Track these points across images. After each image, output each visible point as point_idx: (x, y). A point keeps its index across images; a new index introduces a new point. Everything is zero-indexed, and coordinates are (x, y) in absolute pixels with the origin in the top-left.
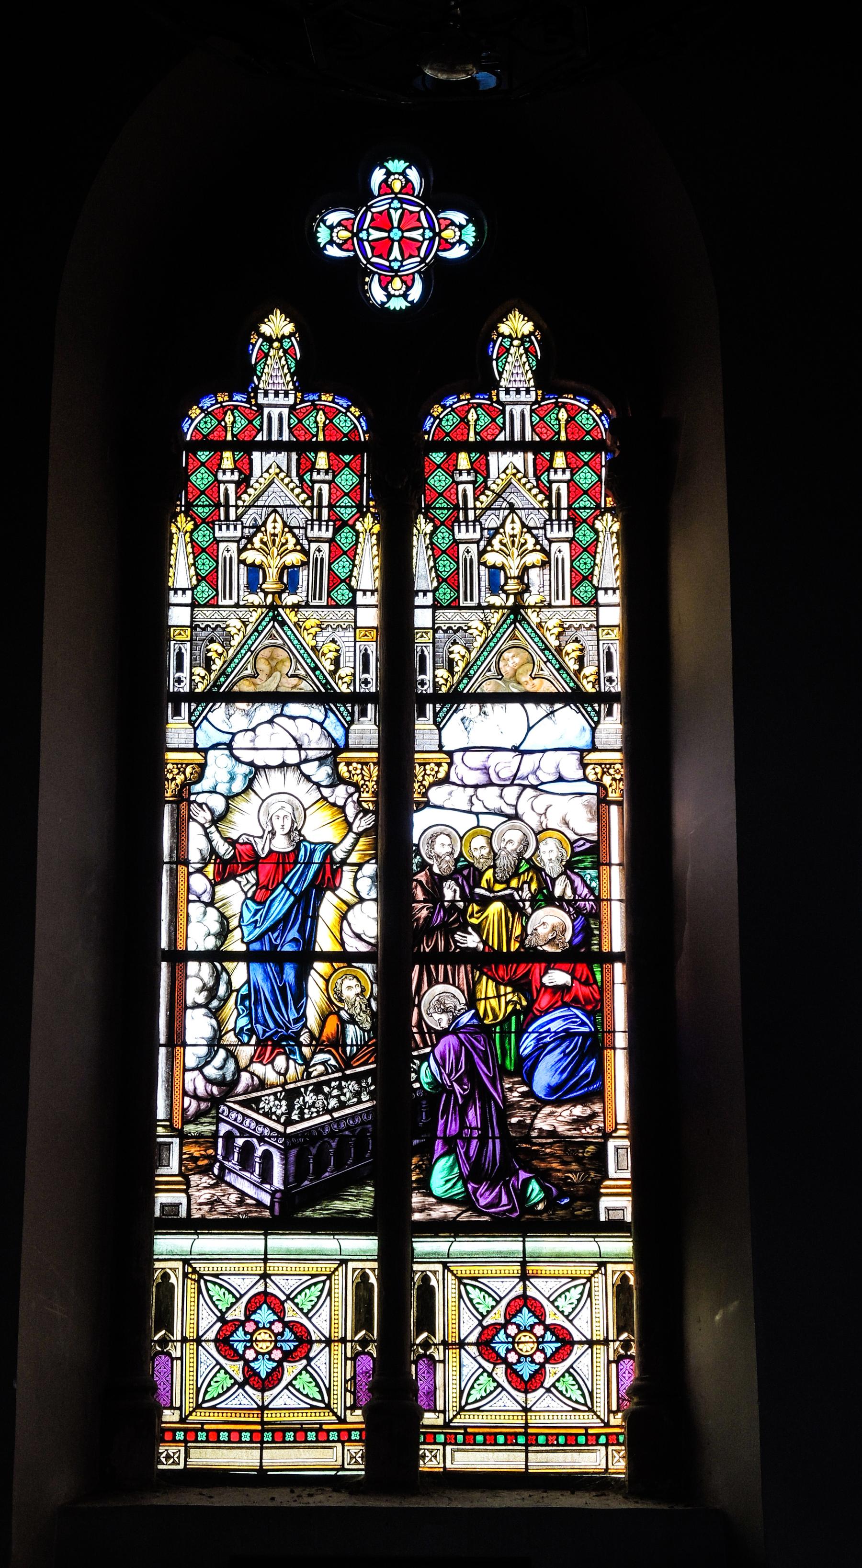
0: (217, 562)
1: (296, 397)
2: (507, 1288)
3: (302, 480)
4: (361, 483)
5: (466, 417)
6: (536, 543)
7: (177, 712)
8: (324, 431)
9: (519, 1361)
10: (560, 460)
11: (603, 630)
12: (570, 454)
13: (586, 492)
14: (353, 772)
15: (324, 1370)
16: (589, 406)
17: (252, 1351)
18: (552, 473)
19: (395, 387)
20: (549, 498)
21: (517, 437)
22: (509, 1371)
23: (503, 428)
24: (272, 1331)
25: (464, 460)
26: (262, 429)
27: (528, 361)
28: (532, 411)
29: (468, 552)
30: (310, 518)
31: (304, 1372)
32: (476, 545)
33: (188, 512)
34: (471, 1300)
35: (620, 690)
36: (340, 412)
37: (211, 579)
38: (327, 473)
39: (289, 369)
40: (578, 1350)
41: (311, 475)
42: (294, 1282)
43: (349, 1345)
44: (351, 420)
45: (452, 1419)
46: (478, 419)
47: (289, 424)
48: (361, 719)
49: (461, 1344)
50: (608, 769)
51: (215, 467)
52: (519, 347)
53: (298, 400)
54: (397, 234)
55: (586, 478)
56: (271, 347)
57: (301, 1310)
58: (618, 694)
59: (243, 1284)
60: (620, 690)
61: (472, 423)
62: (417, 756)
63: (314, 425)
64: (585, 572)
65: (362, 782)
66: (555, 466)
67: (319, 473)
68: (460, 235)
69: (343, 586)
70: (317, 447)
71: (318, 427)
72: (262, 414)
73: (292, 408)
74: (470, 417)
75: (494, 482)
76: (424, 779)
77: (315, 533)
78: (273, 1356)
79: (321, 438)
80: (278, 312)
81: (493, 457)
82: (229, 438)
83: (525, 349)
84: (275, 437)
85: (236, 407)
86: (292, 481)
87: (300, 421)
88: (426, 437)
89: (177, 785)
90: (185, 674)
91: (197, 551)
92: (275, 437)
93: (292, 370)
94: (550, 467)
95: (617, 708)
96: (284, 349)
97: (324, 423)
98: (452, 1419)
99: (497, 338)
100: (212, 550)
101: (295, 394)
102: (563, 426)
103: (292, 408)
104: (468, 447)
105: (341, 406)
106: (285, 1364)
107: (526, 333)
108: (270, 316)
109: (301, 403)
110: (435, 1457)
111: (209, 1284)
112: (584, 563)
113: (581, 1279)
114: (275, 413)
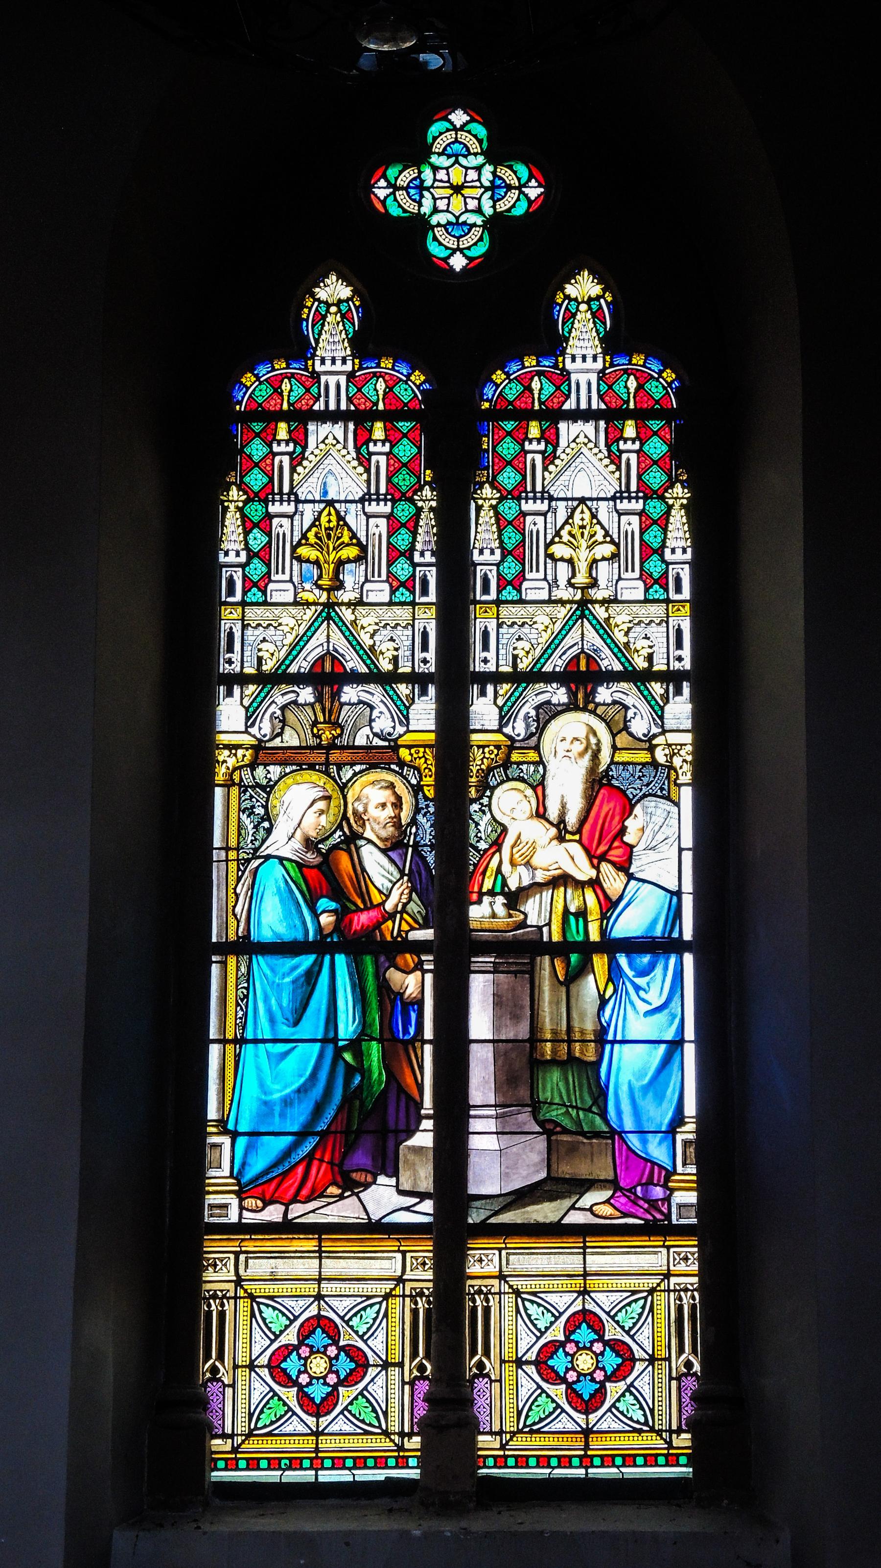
0: (523, 535)
2: (565, 1302)
4: (419, 452)
5: (280, 387)
6: (594, 517)
7: (230, 694)
10: (630, 430)
11: (673, 606)
12: (389, 425)
13: (509, 463)
14: (415, 756)
15: (380, 1394)
17: (306, 1375)
18: (371, 445)
19: (458, 348)
20: (368, 471)
21: (332, 406)
22: (569, 1391)
23: (568, 397)
24: (575, 1353)
25: (534, 430)
26: (320, 396)
27: (345, 328)
29: (535, 524)
30: (618, 489)
32: (543, 518)
34: (529, 1316)
35: (433, 671)
36: (401, 380)
38: (634, 442)
39: (347, 335)
41: (368, 448)
42: (303, 1302)
44: (412, 390)
45: (241, 1444)
46: (291, 390)
47: (599, 391)
49: (519, 1363)
50: (679, 750)
52: (336, 314)
53: (356, 367)
54: (457, 190)
55: (657, 448)
57: (622, 1328)
58: (430, 675)
59: (561, 1301)
60: (433, 671)
61: (285, 394)
62: (474, 737)
63: (375, 393)
64: (656, 546)
65: (425, 765)
66: (530, 436)
69: (655, 557)
72: (319, 382)
73: (351, 376)
74: (283, 387)
76: (483, 763)
78: (328, 1380)
79: (381, 406)
80: (586, 273)
81: (562, 426)
84: (583, 406)
85: (293, 375)
88: (238, 407)
93: (601, 336)
95: (432, 690)
96: (341, 314)
97: (385, 391)
98: (241, 1444)
99: (563, 302)
100: (265, 523)
102: (632, 396)
103: (351, 376)
104: (539, 416)
105: (402, 374)
106: (340, 1389)
107: (593, 295)
108: (577, 277)
111: (262, 1307)
112: (653, 537)
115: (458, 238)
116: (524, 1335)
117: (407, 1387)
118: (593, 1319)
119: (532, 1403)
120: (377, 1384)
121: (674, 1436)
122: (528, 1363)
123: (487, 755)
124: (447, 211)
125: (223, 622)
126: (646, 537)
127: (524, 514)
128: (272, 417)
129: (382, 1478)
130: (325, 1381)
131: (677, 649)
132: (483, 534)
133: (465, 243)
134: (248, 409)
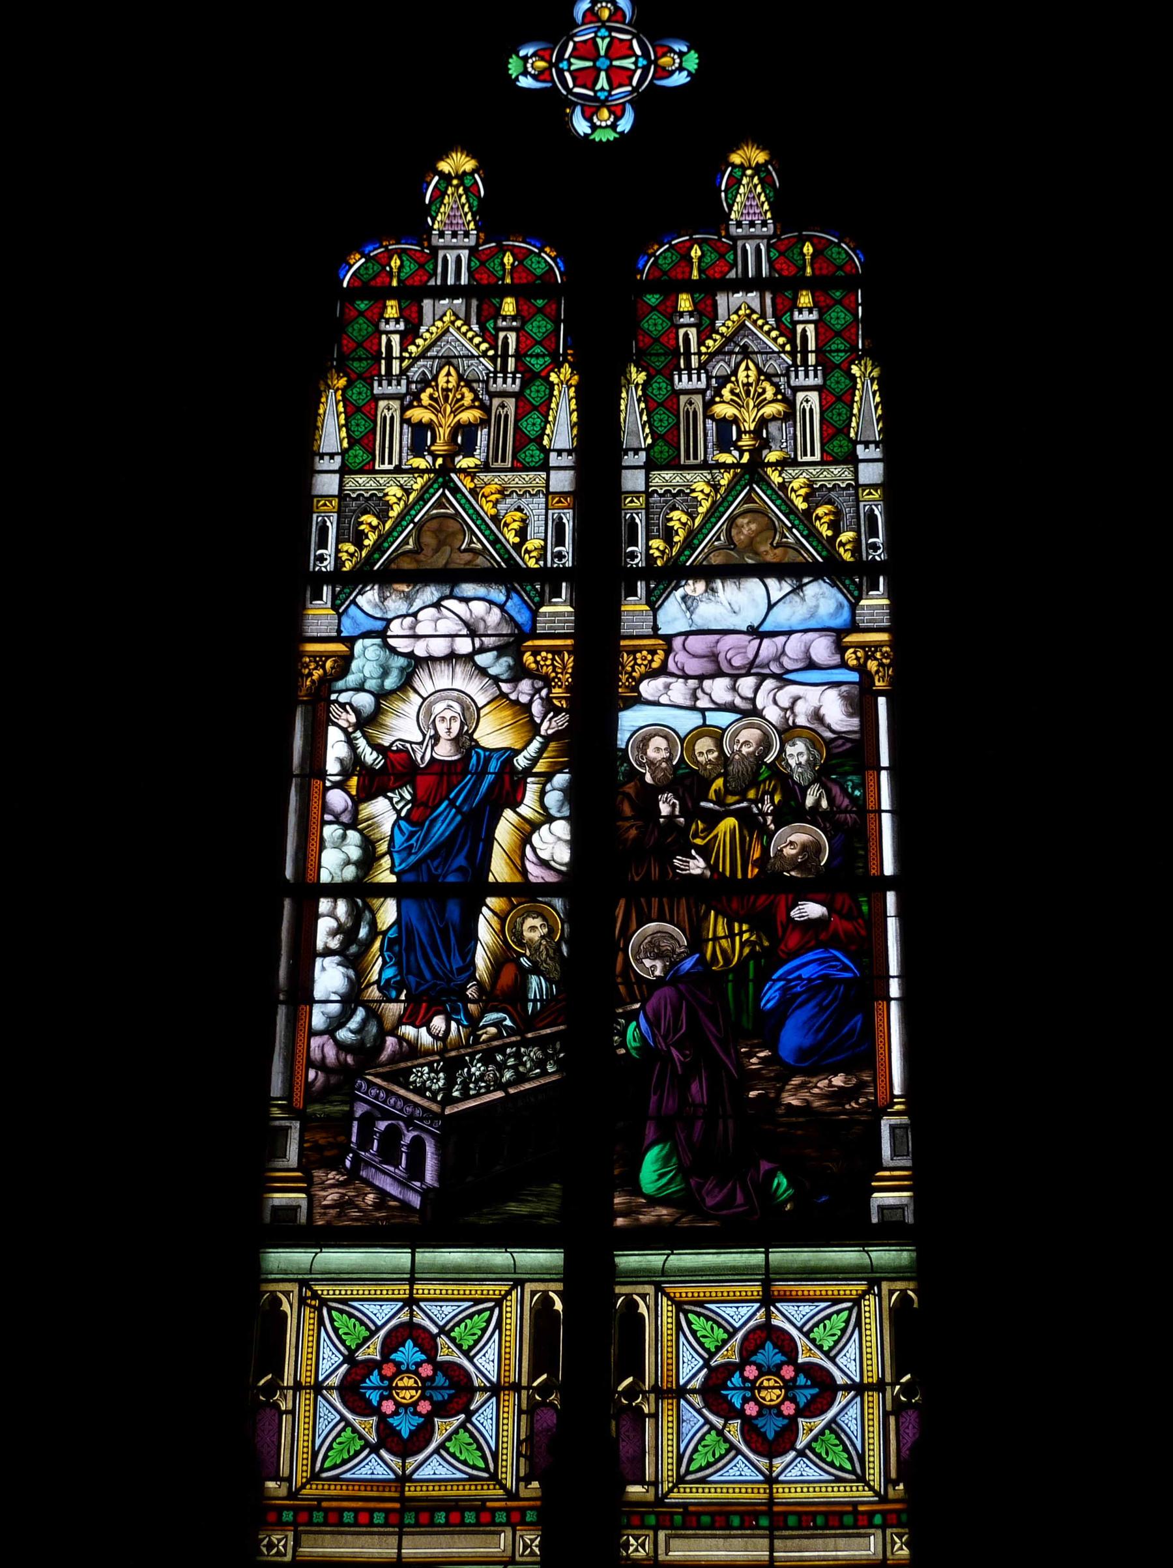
3: (483, 328)
19: (601, 261)
36: (533, 252)
38: (811, 312)
40: (841, 1399)
43: (524, 1393)
56: (744, 174)
67: (800, 312)
68: (682, 67)
69: (533, 446)
70: (506, 291)
73: (473, 251)
74: (693, 254)
76: (634, 670)
97: (512, 265)
101: (477, 235)
104: (690, 287)
114: (451, 256)
116: (327, 1353)
117: (524, 1417)
118: (423, 1335)
119: (699, 1442)
120: (849, 1413)
121: (522, 1484)
122: (484, 1389)
123: (639, 661)
125: (315, 516)
126: (523, 424)
127: (376, 399)
128: (381, 294)
130: (415, 1409)
131: (557, 546)
132: (632, 412)
134: (651, 277)
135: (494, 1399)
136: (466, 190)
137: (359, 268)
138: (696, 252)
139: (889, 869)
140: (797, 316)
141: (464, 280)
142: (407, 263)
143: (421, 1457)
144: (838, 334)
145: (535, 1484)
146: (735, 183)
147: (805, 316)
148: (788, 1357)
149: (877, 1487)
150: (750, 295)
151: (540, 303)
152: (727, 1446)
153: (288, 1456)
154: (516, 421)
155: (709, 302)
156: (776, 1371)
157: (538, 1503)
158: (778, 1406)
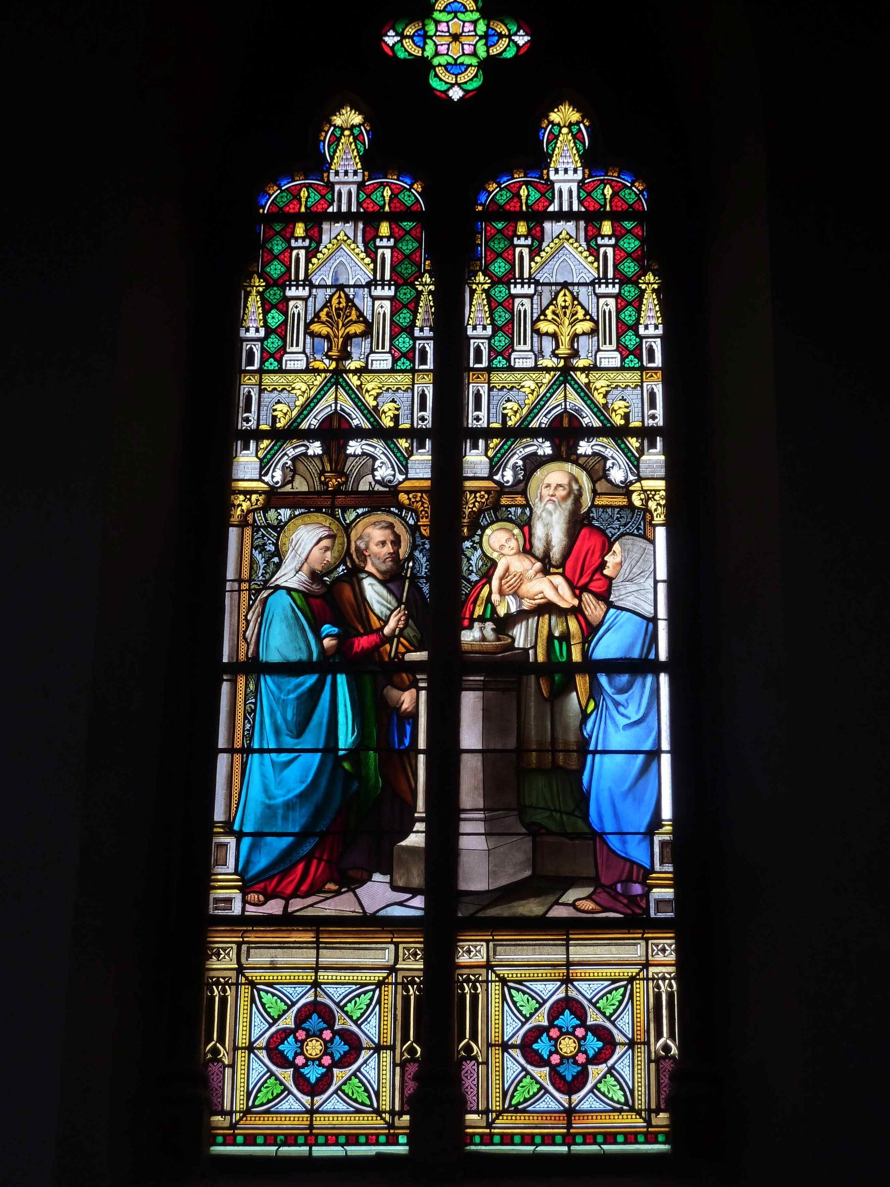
1: (364, 176)
3: (588, 245)
7: (475, 446)
8: (389, 204)
9: (561, 1063)
16: (633, 184)
19: (455, 191)
21: (565, 208)
24: (559, 1037)
28: (579, 188)
31: (608, 1076)
33: (263, 275)
36: (405, 188)
37: (281, 331)
39: (358, 152)
40: (517, 1040)
47: (579, 197)
48: (651, 451)
49: (505, 1047)
50: (654, 495)
51: (287, 236)
52: (349, 136)
53: (366, 178)
56: (342, 134)
59: (545, 989)
61: (303, 200)
67: (381, 240)
69: (630, 333)
70: (605, 216)
71: (605, 199)
73: (361, 186)
74: (521, 192)
75: (326, 247)
77: (602, 290)
81: (547, 225)
82: (303, 209)
83: (572, 135)
84: (565, 208)
86: (580, 245)
87: (368, 196)
88: (261, 211)
89: (242, 511)
90: (483, 414)
91: (492, 304)
92: (344, 209)
94: (377, 236)
97: (390, 197)
99: (547, 126)
100: (283, 305)
101: (363, 173)
109: (368, 180)
110: (228, 954)
111: (262, 993)
113: (626, 980)
114: (344, 190)
115: (456, 76)
121: (653, 1115)
122: (514, 1046)
124: (447, 54)
127: (513, 297)
128: (513, 217)
129: (374, 1153)
131: (476, 411)
133: (462, 79)
135: (376, 1055)
136: (355, 139)
137: (276, 197)
138: (304, 193)
139: (663, 656)
140: (378, 243)
141: (354, 209)
142: (312, 195)
143: (325, 1096)
144: (499, 255)
145: (406, 1118)
146: (554, 138)
147: (385, 242)
148: (585, 1021)
149: (242, 1122)
150: (347, 225)
151: (500, 226)
152: (538, 1086)
153: (229, 1099)
154: (392, 316)
155: (538, 229)
156: (319, 1035)
157: (667, 1129)
158: (574, 1057)
